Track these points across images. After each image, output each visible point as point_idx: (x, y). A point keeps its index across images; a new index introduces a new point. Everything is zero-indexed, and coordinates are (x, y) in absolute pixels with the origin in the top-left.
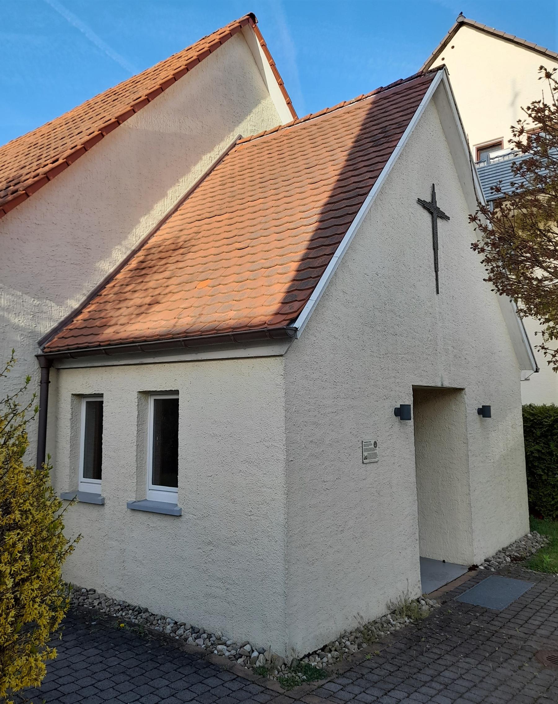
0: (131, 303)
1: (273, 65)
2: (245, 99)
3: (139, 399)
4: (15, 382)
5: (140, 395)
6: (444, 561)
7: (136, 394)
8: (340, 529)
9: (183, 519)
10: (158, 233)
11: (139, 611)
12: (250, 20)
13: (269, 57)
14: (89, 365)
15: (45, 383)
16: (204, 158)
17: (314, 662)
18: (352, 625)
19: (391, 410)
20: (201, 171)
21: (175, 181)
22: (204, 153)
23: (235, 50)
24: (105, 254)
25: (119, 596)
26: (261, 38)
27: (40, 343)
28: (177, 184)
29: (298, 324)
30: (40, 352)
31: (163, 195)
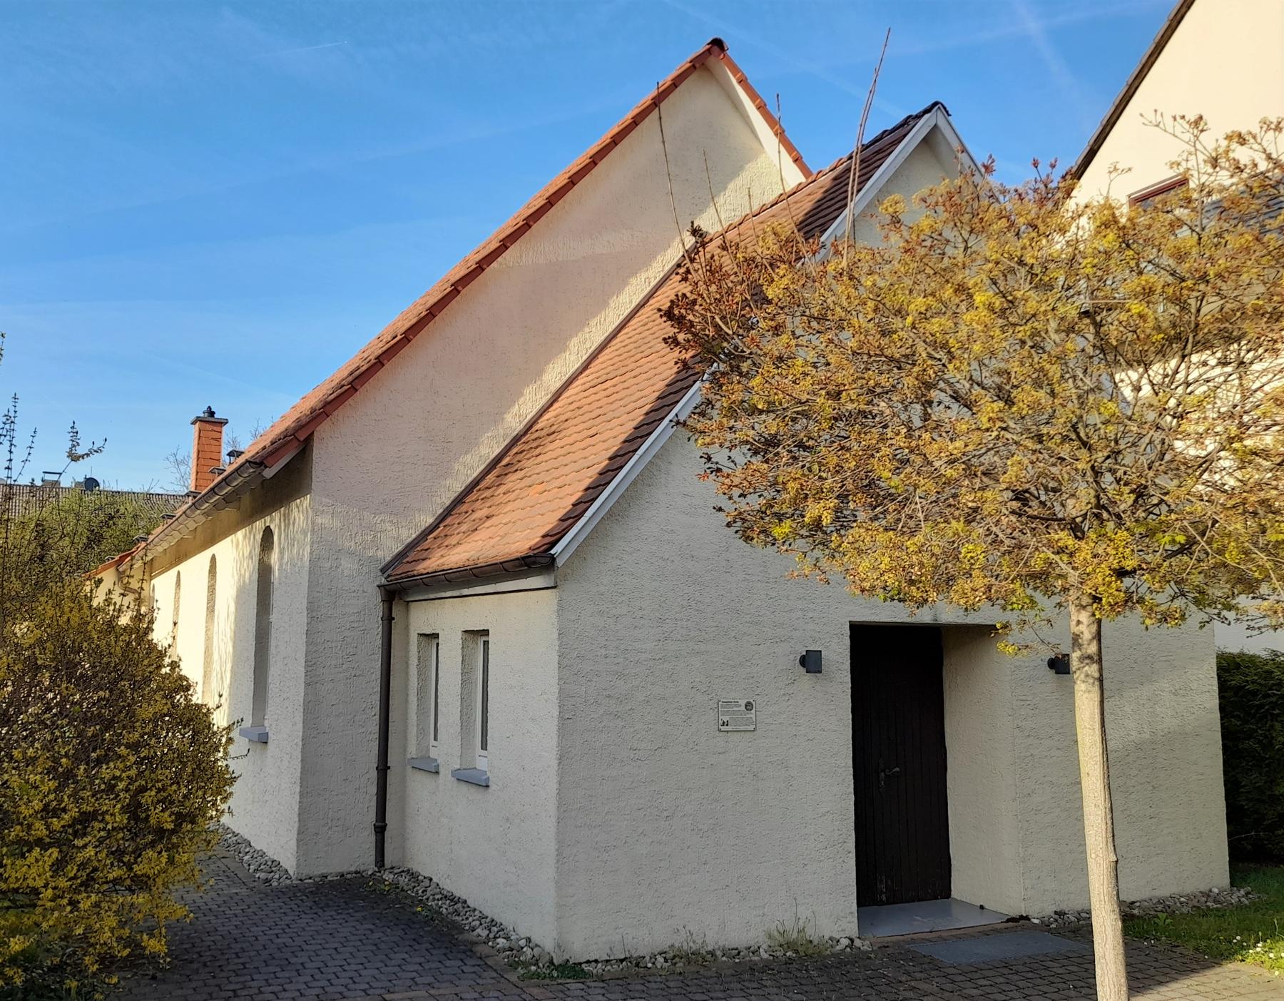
0: (475, 516)
1: (762, 108)
2: (718, 165)
3: (464, 640)
4: (352, 618)
5: (466, 635)
6: (982, 907)
7: (460, 634)
8: (665, 814)
9: (490, 790)
10: (556, 405)
11: (453, 900)
12: (716, 49)
13: (753, 95)
14: (432, 596)
15: (388, 620)
16: (633, 281)
17: (586, 967)
18: (680, 941)
19: (792, 657)
20: (631, 302)
21: (582, 323)
22: (634, 273)
23: (696, 102)
24: (470, 444)
25: (448, 886)
26: (735, 70)
27: (383, 570)
28: (587, 330)
29: (556, 550)
30: (383, 581)
31: (563, 348)
